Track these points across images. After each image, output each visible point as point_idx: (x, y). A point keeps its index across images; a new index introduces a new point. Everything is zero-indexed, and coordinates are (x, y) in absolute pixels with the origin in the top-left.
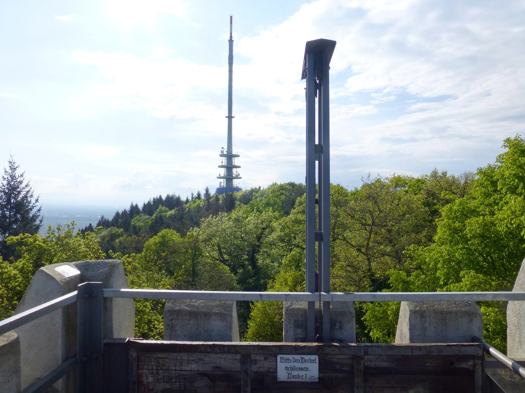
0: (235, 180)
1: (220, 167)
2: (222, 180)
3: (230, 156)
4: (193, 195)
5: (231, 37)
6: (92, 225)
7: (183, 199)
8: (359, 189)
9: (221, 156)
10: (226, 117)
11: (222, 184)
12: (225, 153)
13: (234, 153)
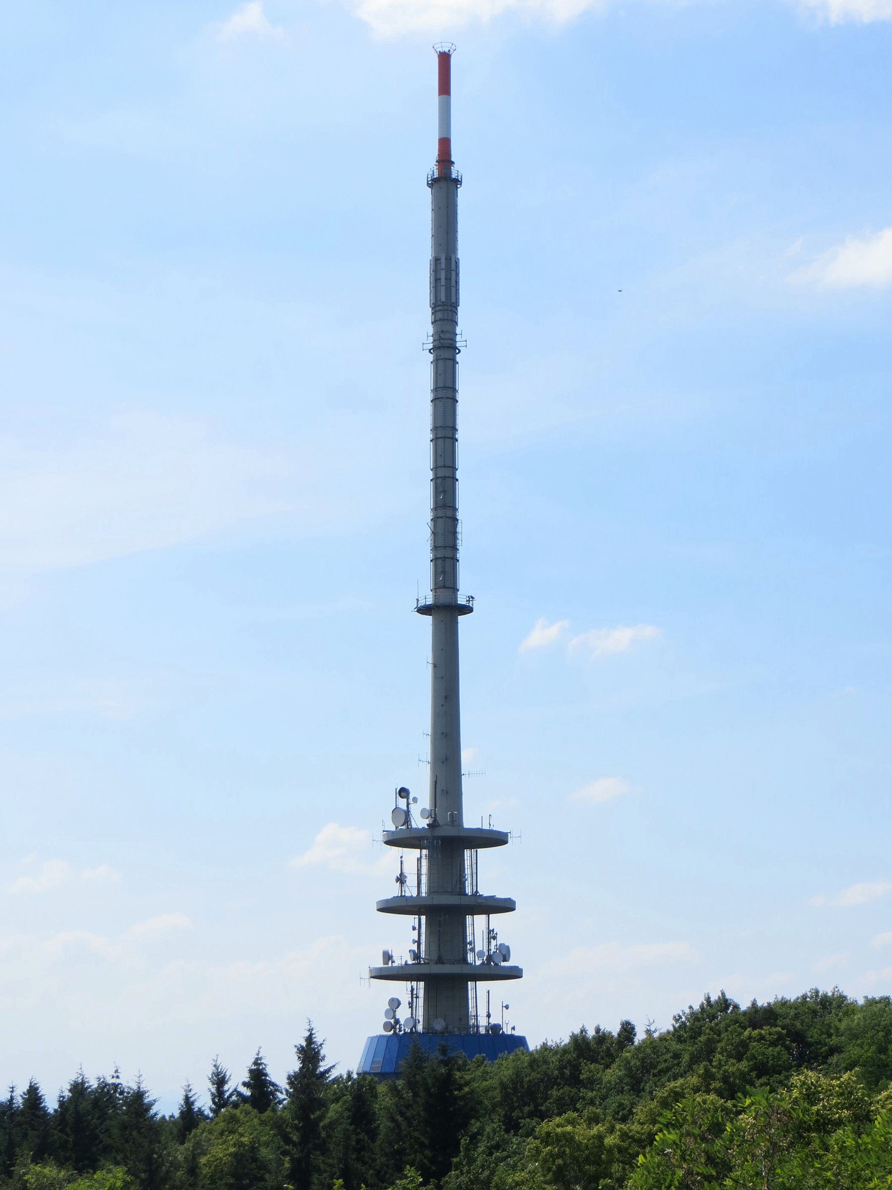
0: (483, 986)
1: (390, 907)
2: (401, 989)
3: (447, 842)
4: (220, 1080)
5: (445, 159)
6: (42, 1091)
7: (166, 1106)
8: (344, 1059)
9: (393, 841)
10: (424, 610)
11: (403, 1014)
12: (420, 822)
13: (471, 820)
